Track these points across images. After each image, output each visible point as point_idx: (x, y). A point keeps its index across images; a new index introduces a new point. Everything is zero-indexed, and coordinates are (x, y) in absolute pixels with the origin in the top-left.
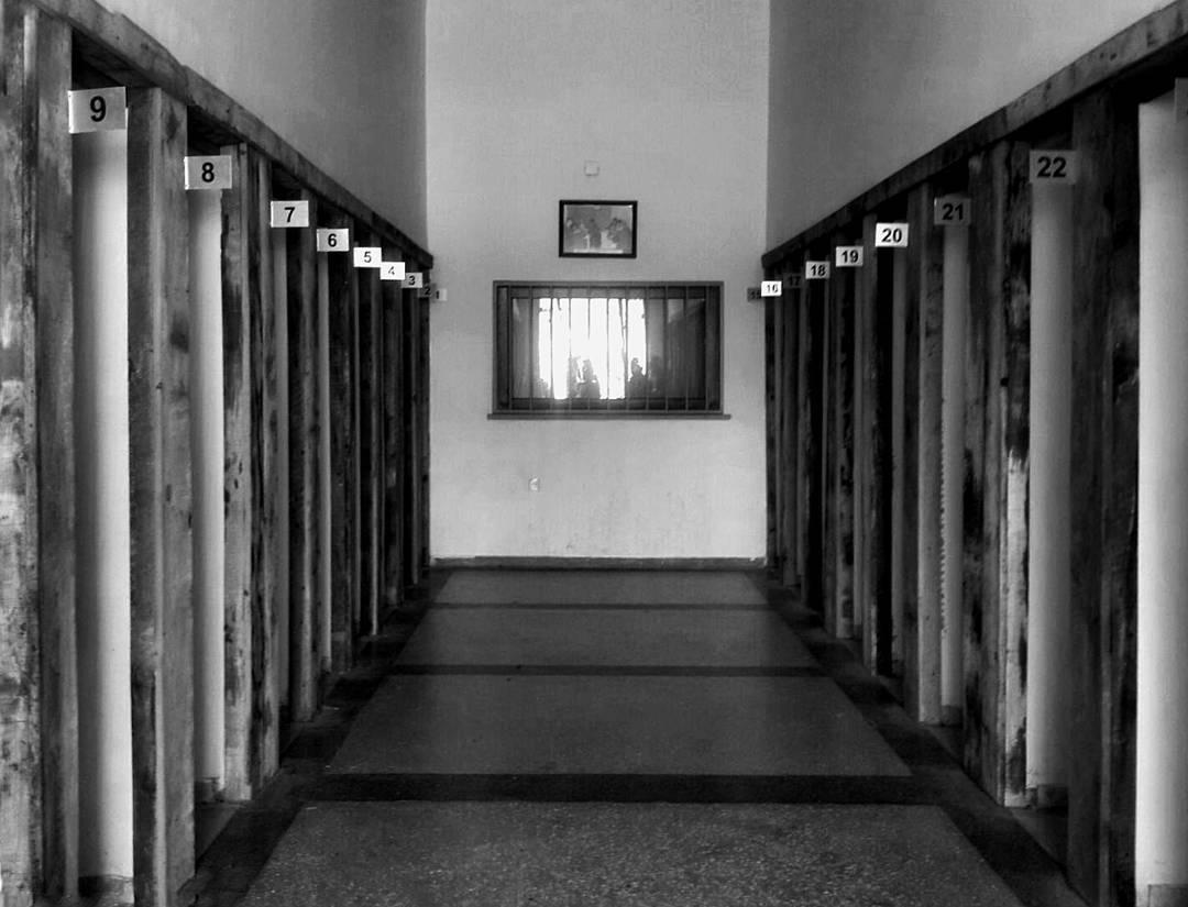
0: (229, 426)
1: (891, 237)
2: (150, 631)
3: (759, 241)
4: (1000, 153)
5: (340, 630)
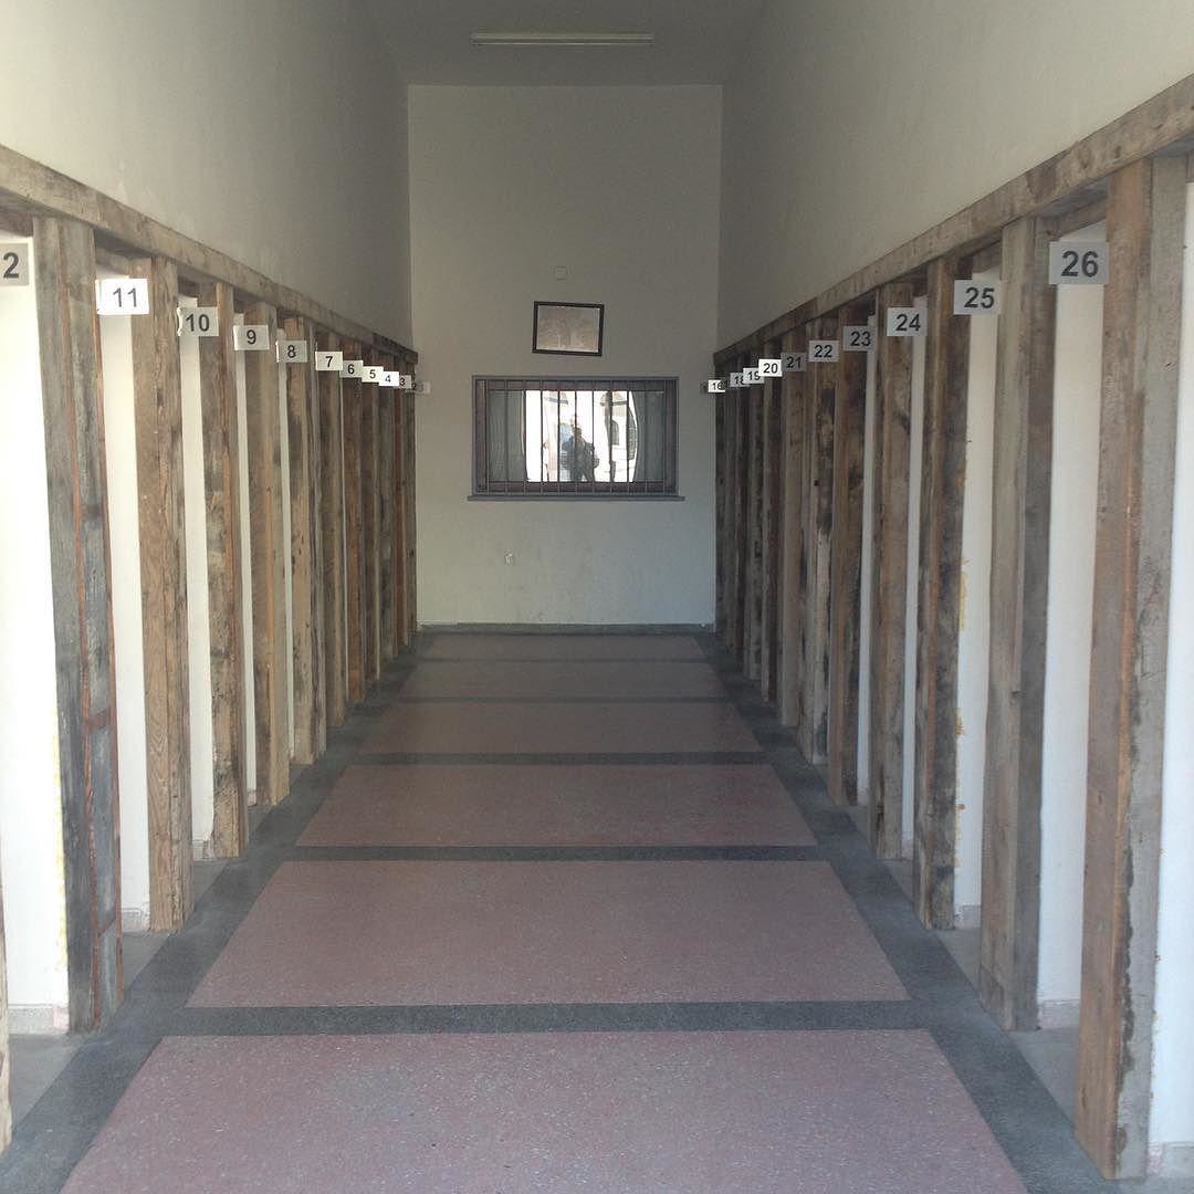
0: (294, 513)
1: (770, 370)
2: (266, 639)
3: (711, 342)
4: (818, 322)
5: (356, 668)
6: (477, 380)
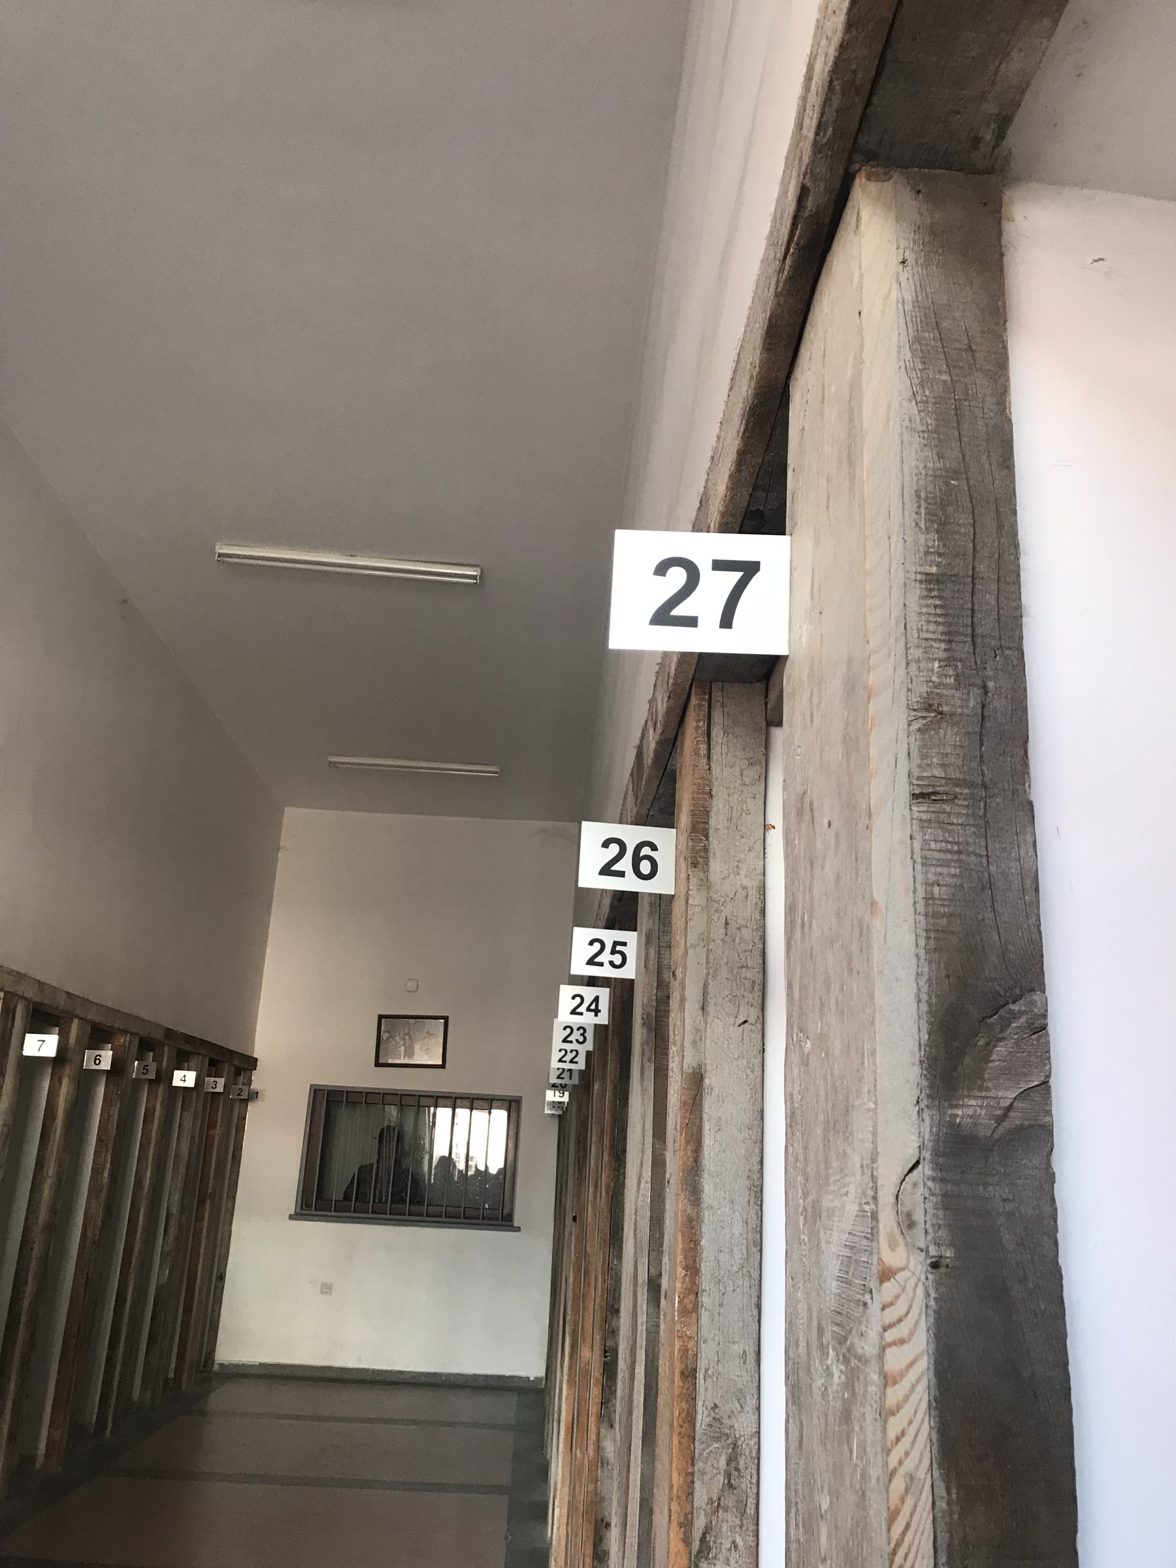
6: (317, 1093)
